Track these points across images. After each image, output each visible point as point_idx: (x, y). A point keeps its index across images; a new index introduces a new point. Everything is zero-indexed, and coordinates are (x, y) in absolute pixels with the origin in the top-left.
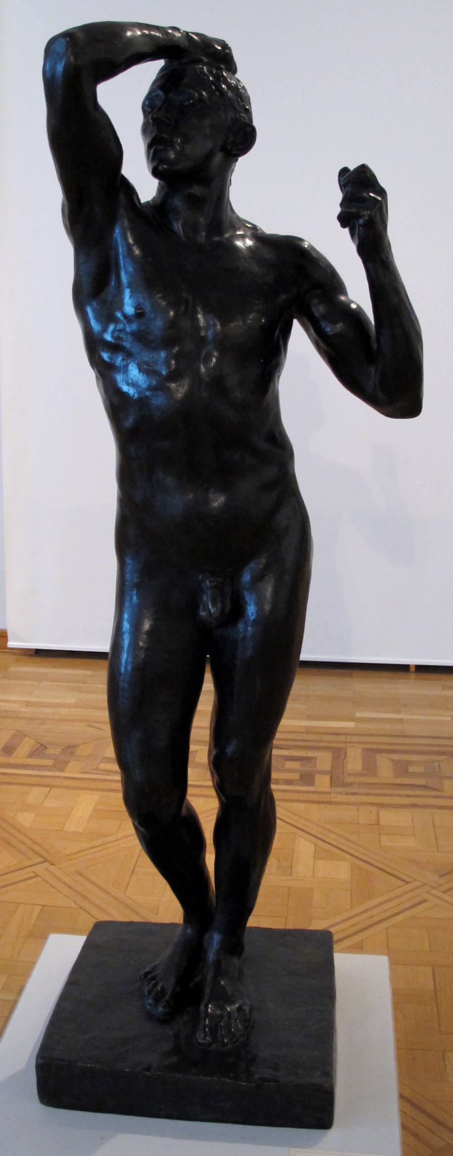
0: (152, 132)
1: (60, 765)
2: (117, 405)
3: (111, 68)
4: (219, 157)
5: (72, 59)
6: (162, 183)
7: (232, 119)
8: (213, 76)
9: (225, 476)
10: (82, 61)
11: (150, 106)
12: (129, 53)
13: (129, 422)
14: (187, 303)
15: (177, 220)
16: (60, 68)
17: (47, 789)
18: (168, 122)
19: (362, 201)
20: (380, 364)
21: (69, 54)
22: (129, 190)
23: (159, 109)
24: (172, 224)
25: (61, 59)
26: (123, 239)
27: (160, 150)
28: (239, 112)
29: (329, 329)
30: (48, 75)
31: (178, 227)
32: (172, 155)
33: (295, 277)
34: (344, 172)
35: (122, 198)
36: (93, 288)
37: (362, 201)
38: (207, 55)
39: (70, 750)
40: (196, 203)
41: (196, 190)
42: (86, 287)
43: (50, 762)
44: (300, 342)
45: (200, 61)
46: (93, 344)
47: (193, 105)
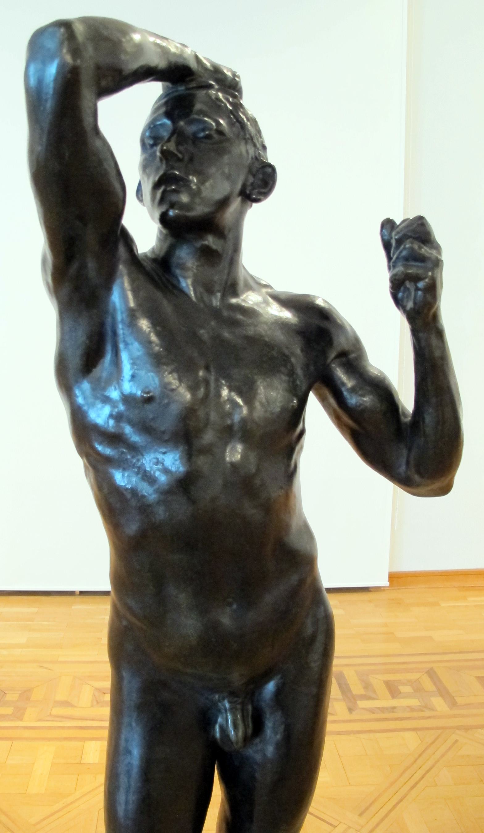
0: (158, 169)
1: (19, 714)
2: (114, 505)
3: (116, 79)
4: (236, 203)
5: (68, 59)
6: (164, 231)
7: (252, 158)
8: (231, 104)
9: (248, 590)
10: (80, 69)
11: (152, 138)
12: (134, 65)
13: (132, 528)
14: (207, 382)
15: (185, 278)
16: (52, 70)
17: (9, 743)
18: (180, 156)
19: (412, 259)
20: (415, 442)
21: (65, 51)
22: (126, 239)
23: (169, 140)
24: (179, 281)
25: (52, 59)
26: (122, 296)
27: (174, 191)
28: (258, 149)
29: (352, 400)
30: (33, 82)
31: (187, 284)
32: (184, 198)
33: (318, 343)
34: (388, 225)
35: (122, 250)
36: (85, 355)
37: (412, 259)
38: (218, 81)
39: (26, 694)
40: (209, 256)
41: (210, 241)
42: (75, 360)
43: (9, 711)
44: (317, 415)
45: (210, 87)
46: (84, 431)
47: (208, 137)
